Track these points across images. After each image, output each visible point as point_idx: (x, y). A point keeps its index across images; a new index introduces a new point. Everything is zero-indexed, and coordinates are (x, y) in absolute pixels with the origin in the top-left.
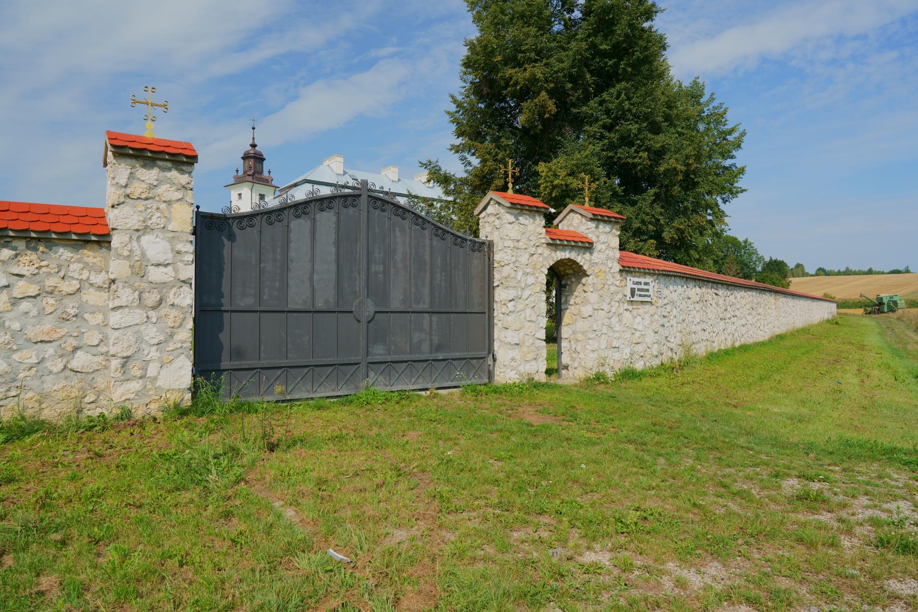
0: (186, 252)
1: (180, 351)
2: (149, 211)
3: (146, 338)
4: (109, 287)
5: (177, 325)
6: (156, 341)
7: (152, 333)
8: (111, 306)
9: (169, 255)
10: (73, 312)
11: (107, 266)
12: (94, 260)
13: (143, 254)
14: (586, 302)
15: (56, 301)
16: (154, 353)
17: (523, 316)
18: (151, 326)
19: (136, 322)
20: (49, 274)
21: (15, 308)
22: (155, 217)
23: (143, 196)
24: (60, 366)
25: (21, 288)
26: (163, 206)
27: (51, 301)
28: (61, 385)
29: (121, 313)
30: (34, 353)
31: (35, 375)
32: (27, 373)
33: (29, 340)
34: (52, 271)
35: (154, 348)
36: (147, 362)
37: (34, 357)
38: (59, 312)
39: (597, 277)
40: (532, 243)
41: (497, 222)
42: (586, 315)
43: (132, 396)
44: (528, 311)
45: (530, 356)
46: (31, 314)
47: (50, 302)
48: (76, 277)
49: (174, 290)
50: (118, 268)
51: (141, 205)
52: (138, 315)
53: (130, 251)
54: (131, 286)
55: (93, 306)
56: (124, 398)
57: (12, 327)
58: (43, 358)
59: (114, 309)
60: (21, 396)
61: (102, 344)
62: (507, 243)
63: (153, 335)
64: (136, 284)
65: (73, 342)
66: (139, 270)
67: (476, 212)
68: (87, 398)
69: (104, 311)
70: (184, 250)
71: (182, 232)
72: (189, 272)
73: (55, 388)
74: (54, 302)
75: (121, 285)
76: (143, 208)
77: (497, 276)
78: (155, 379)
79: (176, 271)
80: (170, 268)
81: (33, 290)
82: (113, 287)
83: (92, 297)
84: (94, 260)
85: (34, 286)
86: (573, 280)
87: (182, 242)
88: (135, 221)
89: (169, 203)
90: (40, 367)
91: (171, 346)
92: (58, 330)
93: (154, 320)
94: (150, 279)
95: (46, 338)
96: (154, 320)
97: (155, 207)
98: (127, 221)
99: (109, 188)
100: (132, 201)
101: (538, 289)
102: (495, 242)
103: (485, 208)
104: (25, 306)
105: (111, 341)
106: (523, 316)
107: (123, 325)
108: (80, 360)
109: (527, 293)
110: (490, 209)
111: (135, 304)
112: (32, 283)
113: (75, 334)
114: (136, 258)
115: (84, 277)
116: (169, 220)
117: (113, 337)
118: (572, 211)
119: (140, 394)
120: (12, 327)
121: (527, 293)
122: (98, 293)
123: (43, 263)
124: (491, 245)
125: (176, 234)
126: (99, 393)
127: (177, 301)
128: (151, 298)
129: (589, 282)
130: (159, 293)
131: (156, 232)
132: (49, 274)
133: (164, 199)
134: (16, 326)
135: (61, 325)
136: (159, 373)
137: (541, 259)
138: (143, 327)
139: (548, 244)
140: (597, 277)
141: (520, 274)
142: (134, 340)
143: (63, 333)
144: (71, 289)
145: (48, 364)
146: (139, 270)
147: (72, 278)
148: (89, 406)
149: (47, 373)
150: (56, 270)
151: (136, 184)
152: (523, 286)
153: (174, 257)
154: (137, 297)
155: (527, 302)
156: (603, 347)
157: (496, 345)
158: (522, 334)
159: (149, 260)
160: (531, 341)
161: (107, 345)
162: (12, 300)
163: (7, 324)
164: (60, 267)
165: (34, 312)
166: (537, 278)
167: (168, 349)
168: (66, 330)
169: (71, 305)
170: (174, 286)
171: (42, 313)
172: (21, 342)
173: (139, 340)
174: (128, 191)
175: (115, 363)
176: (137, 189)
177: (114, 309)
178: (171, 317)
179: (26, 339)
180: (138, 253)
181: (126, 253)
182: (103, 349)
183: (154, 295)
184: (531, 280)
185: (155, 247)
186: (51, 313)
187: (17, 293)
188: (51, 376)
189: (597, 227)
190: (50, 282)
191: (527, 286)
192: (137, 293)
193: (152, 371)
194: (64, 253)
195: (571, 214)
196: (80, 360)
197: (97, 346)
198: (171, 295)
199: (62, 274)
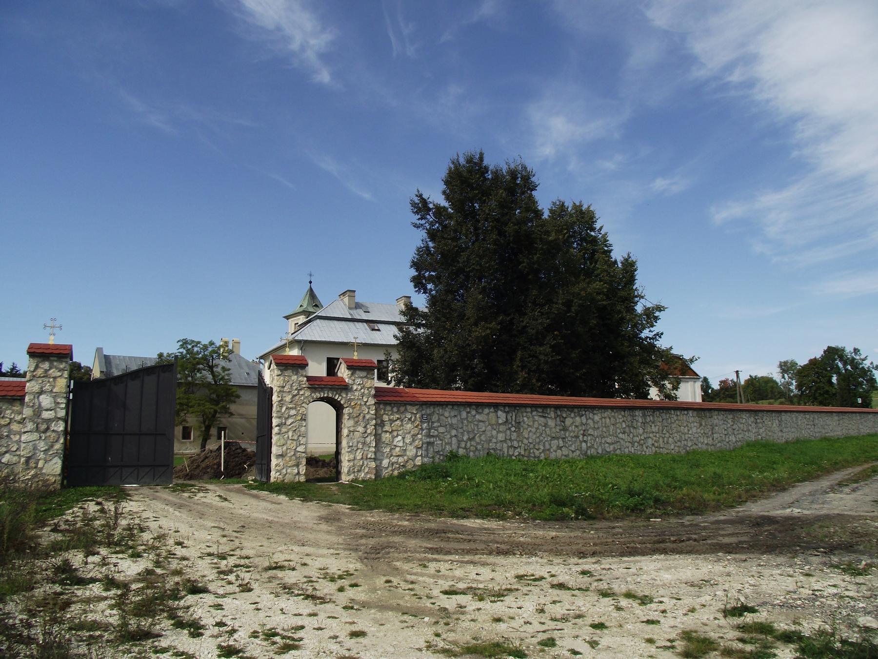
7: (42, 446)
16: (42, 456)
50: (27, 412)
52: (35, 436)
72: (62, 413)
78: (42, 469)
79: (56, 413)
83: (15, 427)
89: (55, 378)
128: (43, 427)
173: (35, 448)
176: (40, 372)
182: (18, 453)
185: (46, 401)
193: (40, 465)
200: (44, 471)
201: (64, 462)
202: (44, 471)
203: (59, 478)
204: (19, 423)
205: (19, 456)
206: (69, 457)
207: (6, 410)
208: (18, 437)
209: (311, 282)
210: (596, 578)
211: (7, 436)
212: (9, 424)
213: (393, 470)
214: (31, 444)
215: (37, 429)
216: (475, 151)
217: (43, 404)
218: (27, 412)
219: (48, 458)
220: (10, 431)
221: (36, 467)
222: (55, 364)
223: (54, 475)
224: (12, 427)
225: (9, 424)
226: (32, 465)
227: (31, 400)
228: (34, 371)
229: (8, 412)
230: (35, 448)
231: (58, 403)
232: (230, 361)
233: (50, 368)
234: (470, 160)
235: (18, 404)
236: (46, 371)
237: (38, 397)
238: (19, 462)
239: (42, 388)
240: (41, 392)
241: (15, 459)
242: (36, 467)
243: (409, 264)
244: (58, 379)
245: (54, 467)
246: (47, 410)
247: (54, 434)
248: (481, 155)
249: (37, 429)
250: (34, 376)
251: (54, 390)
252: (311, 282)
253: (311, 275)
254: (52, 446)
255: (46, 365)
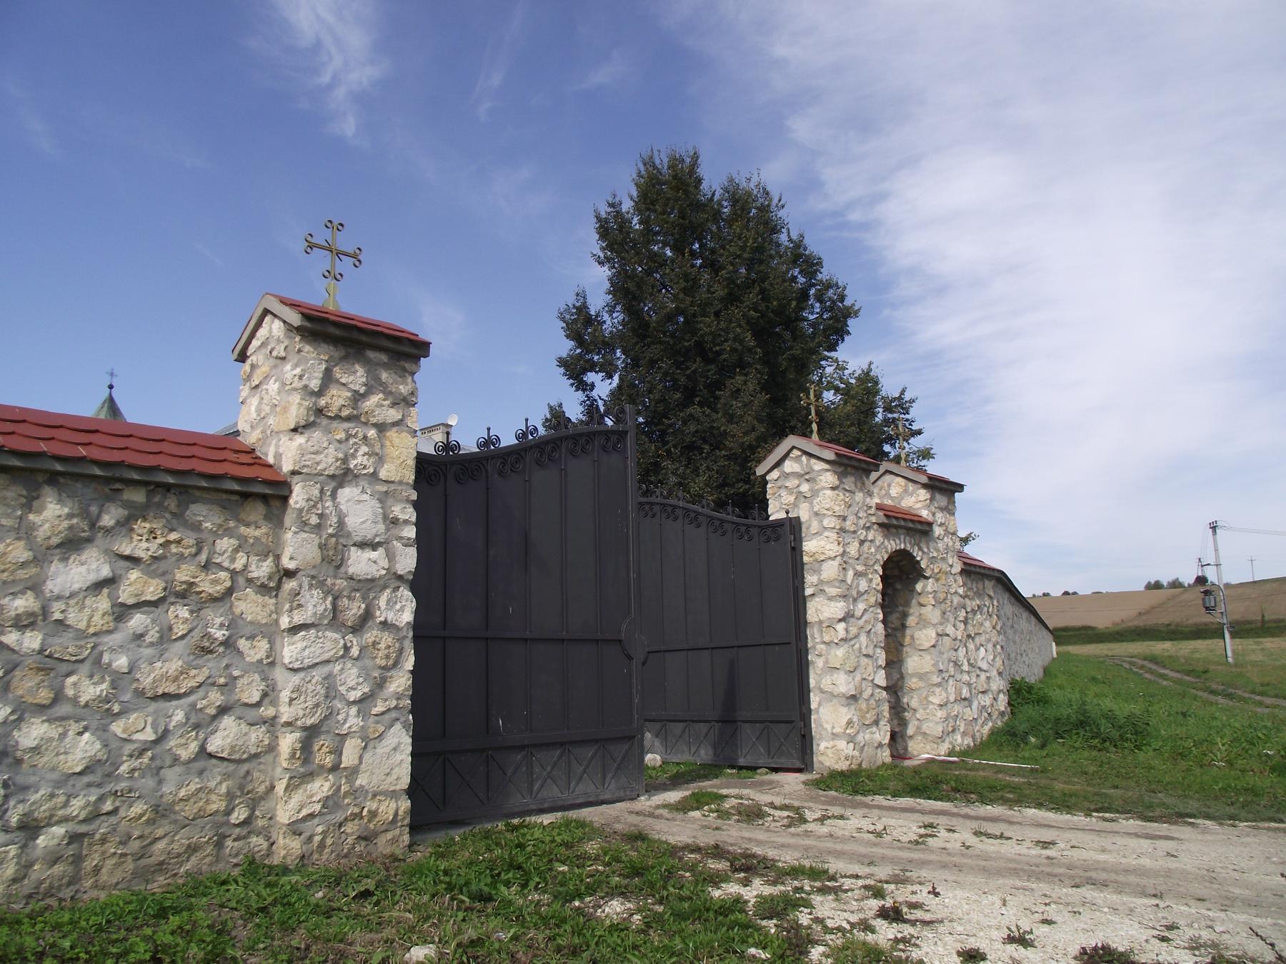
0: (406, 522)
1: (394, 715)
3: (342, 689)
4: (278, 587)
5: (391, 662)
7: (352, 681)
9: (377, 528)
10: (220, 634)
13: (341, 523)
15: (192, 612)
16: (352, 720)
17: (857, 646)
19: (326, 656)
20: (181, 557)
21: (121, 625)
22: (360, 453)
23: (345, 413)
24: (194, 746)
25: (135, 585)
28: (193, 787)
29: (304, 639)
30: (150, 720)
31: (148, 766)
32: (136, 763)
34: (186, 552)
36: (343, 737)
37: (149, 729)
38: (197, 634)
39: (937, 580)
41: (805, 488)
45: (870, 717)
46: (148, 639)
48: (226, 564)
50: (297, 548)
52: (330, 642)
53: (321, 516)
54: (321, 584)
55: (251, 623)
56: (304, 812)
57: (115, 665)
59: (294, 630)
60: (122, 813)
61: (267, 701)
63: (352, 684)
64: (329, 581)
66: (333, 554)
67: (760, 471)
69: (269, 632)
70: (402, 517)
71: (400, 483)
72: (407, 561)
73: (182, 793)
74: (187, 615)
75: (306, 581)
77: (810, 579)
78: (354, 771)
79: (391, 556)
80: (381, 550)
81: (153, 590)
83: (250, 606)
84: (257, 533)
85: (154, 582)
86: (898, 586)
87: (400, 501)
89: (381, 428)
90: (158, 749)
91: (379, 708)
92: (193, 672)
93: (355, 651)
94: (351, 571)
95: (172, 689)
96: (355, 651)
97: (360, 435)
98: (318, 458)
99: (269, 405)
100: (324, 422)
103: (778, 464)
104: (138, 621)
105: (285, 695)
106: (857, 646)
107: (307, 662)
109: (861, 606)
110: (789, 466)
112: (152, 574)
113: (222, 681)
114: (330, 531)
115: (238, 565)
116: (380, 459)
117: (290, 686)
118: (887, 472)
123: (173, 536)
124: (792, 527)
125: (392, 487)
126: (253, 805)
127: (390, 616)
128: (354, 609)
129: (929, 589)
130: (364, 598)
131: (363, 483)
132: (181, 557)
133: (373, 420)
134: (122, 662)
135: (200, 662)
138: (338, 668)
139: (881, 525)
140: (937, 580)
141: (850, 573)
143: (200, 679)
145: (172, 743)
148: (237, 830)
149: (168, 762)
150: (193, 550)
151: (334, 391)
153: (388, 530)
154: (329, 606)
155: (861, 622)
156: (952, 699)
157: (814, 700)
158: (858, 678)
159: (349, 535)
160: (869, 691)
161: (274, 703)
165: (153, 636)
166: (871, 580)
168: (206, 672)
169: (218, 621)
170: (385, 587)
172: (127, 697)
173: (331, 691)
174: (322, 402)
176: (337, 399)
177: (294, 630)
179: (136, 690)
180: (334, 519)
181: (314, 520)
183: (356, 604)
184: (863, 585)
185: (358, 509)
187: (126, 594)
188: (178, 769)
190: (183, 574)
191: (860, 594)
193: (349, 757)
194: (206, 516)
195: (888, 478)
197: (258, 705)
198: (382, 602)
199: (203, 557)
203: (405, 804)
204: (263, 589)
205: (271, 722)
207: (216, 535)
208: (263, 645)
209: (111, 387)
210: (860, 882)
211: (227, 643)
212: (230, 592)
214: (317, 674)
215: (334, 619)
217: (352, 522)
218: (297, 548)
219: (375, 728)
220: (233, 624)
221: (335, 768)
222: (384, 376)
223: (393, 795)
225: (230, 592)
227: (313, 504)
228: (320, 393)
229: (225, 544)
230: (331, 691)
231: (395, 522)
232: (919, 432)
234: (675, 162)
235: (256, 512)
236: (358, 397)
237: (334, 496)
238: (272, 748)
239: (345, 460)
240: (344, 476)
241: (257, 735)
242: (335, 768)
243: (433, 350)
244: (391, 433)
247: (386, 639)
248: (695, 157)
249: (334, 619)
250: (319, 412)
251: (383, 474)
252: (111, 387)
253: (112, 374)
254: (380, 684)
255: (356, 377)
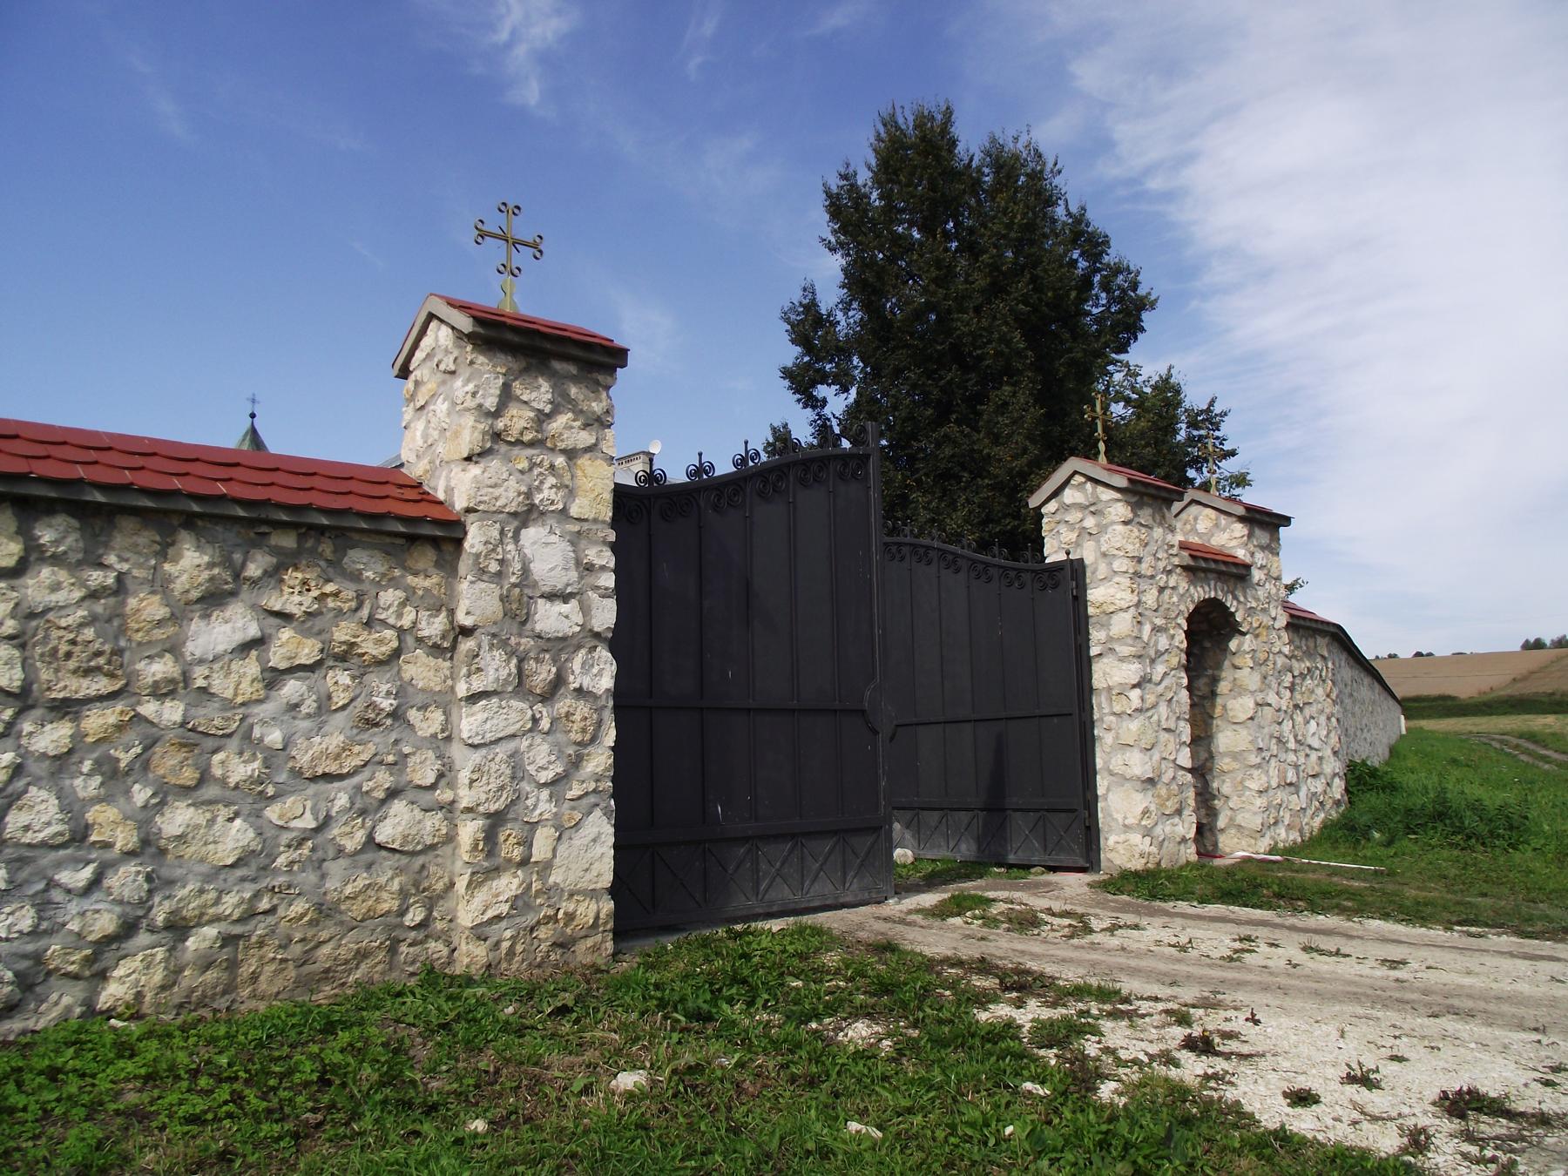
0: (603, 568)
1: (592, 799)
2: (536, 471)
3: (531, 769)
4: (453, 648)
5: (588, 737)
6: (545, 776)
7: (542, 759)
8: (462, 689)
9: (568, 575)
10: (387, 704)
11: (452, 594)
12: (427, 583)
13: (526, 571)
14: (1238, 689)
15: (353, 678)
16: (543, 805)
17: (1155, 718)
18: (538, 740)
20: (339, 613)
21: (273, 693)
22: (547, 485)
23: (527, 437)
24: (360, 836)
25: (288, 646)
26: (560, 461)
27: (344, 678)
29: (484, 709)
30: (309, 804)
31: (309, 858)
32: (295, 855)
33: (297, 773)
34: (346, 607)
35: (545, 794)
36: (533, 826)
37: (308, 815)
38: (360, 704)
39: (1257, 636)
40: (1161, 565)
41: (1090, 522)
42: (1242, 717)
43: (505, 908)
44: (1163, 709)
45: (1171, 806)
46: (304, 709)
47: (340, 680)
48: (391, 621)
49: (581, 655)
50: (475, 600)
51: (522, 459)
52: (515, 713)
53: (502, 562)
54: (504, 644)
55: (423, 690)
56: (490, 914)
58: (328, 818)
59: (473, 698)
60: (281, 912)
61: (443, 782)
62: (1118, 565)
65: (384, 779)
67: (1034, 502)
68: (409, 916)
69: (444, 700)
70: (598, 562)
71: (595, 521)
72: (605, 615)
73: (349, 890)
74: (348, 681)
75: (485, 640)
76: (524, 465)
78: (547, 866)
79: (585, 610)
80: (574, 603)
81: (308, 652)
82: (467, 645)
83: (421, 670)
84: (427, 583)
86: (1207, 644)
87: (596, 543)
88: (512, 494)
89: (571, 454)
90: (320, 839)
91: (576, 791)
92: (357, 749)
93: (545, 724)
94: (538, 628)
95: (333, 768)
96: (545, 724)
98: (497, 492)
99: (434, 429)
101: (1175, 661)
102: (1087, 562)
103: (1056, 493)
104: (292, 688)
105: (464, 776)
106: (1155, 718)
107: (489, 737)
108: (396, 824)
109: (1160, 669)
110: (1069, 496)
111: (510, 689)
112: (307, 633)
113: (391, 759)
114: (513, 579)
115: (406, 622)
116: (571, 493)
117: (470, 766)
118: (1193, 502)
119: (520, 903)
120: (267, 740)
121: (1160, 669)
122: (432, 661)
125: (586, 526)
127: (586, 682)
128: (543, 673)
129: (1246, 647)
130: (555, 661)
131: (551, 521)
132: (339, 613)
133: (561, 445)
134: (274, 737)
135: (365, 736)
136: (554, 850)
137: (1175, 599)
138: (525, 743)
139: (1186, 568)
140: (1257, 636)
142: (508, 772)
143: (366, 757)
144: (383, 651)
146: (517, 610)
147: (383, 622)
149: (331, 854)
150: (353, 604)
151: (513, 410)
152: (1152, 653)
153: (581, 578)
154: (514, 670)
156: (1274, 784)
158: (1156, 757)
159: (535, 585)
161: (452, 785)
162: (267, 675)
163: (257, 733)
164: (360, 598)
165: (309, 706)
167: (569, 795)
168: (371, 748)
170: (579, 647)
171: (325, 707)
172: (282, 777)
175: (469, 831)
176: (517, 420)
177: (473, 698)
178: (577, 717)
180: (517, 566)
181: (494, 567)
182: (444, 795)
183: (545, 667)
184: (1163, 642)
185: (546, 554)
186: (344, 707)
187: (277, 658)
189: (1250, 536)
190: (342, 633)
191: (1159, 654)
192: (514, 661)
195: (1194, 509)
196: (396, 824)
197: (433, 787)
199: (365, 613)
200: (555, 877)
201: (619, 828)
202: (555, 877)
203: (608, 906)
204: (436, 650)
205: (449, 808)
206: (638, 799)
209: (253, 416)
211: (395, 715)
212: (397, 653)
213: (257, 895)
214: (502, 751)
216: (933, 103)
217: (539, 569)
218: (475, 600)
219: (570, 815)
220: (402, 692)
221: (524, 862)
222: (573, 391)
223: (593, 894)
224: (409, 671)
225: (397, 653)
226: (510, 849)
228: (496, 414)
229: (390, 597)
231: (590, 568)
233: (556, 411)
234: (922, 121)
235: (425, 558)
237: (516, 537)
238: (450, 838)
239: (529, 495)
240: (527, 514)
241: (433, 824)
242: (524, 862)
244: (583, 461)
245: (587, 855)
246: (551, 596)
248: (948, 113)
249: (520, 686)
250: (497, 436)
252: (253, 416)
253: (253, 401)
254: (576, 763)
255: (540, 393)
